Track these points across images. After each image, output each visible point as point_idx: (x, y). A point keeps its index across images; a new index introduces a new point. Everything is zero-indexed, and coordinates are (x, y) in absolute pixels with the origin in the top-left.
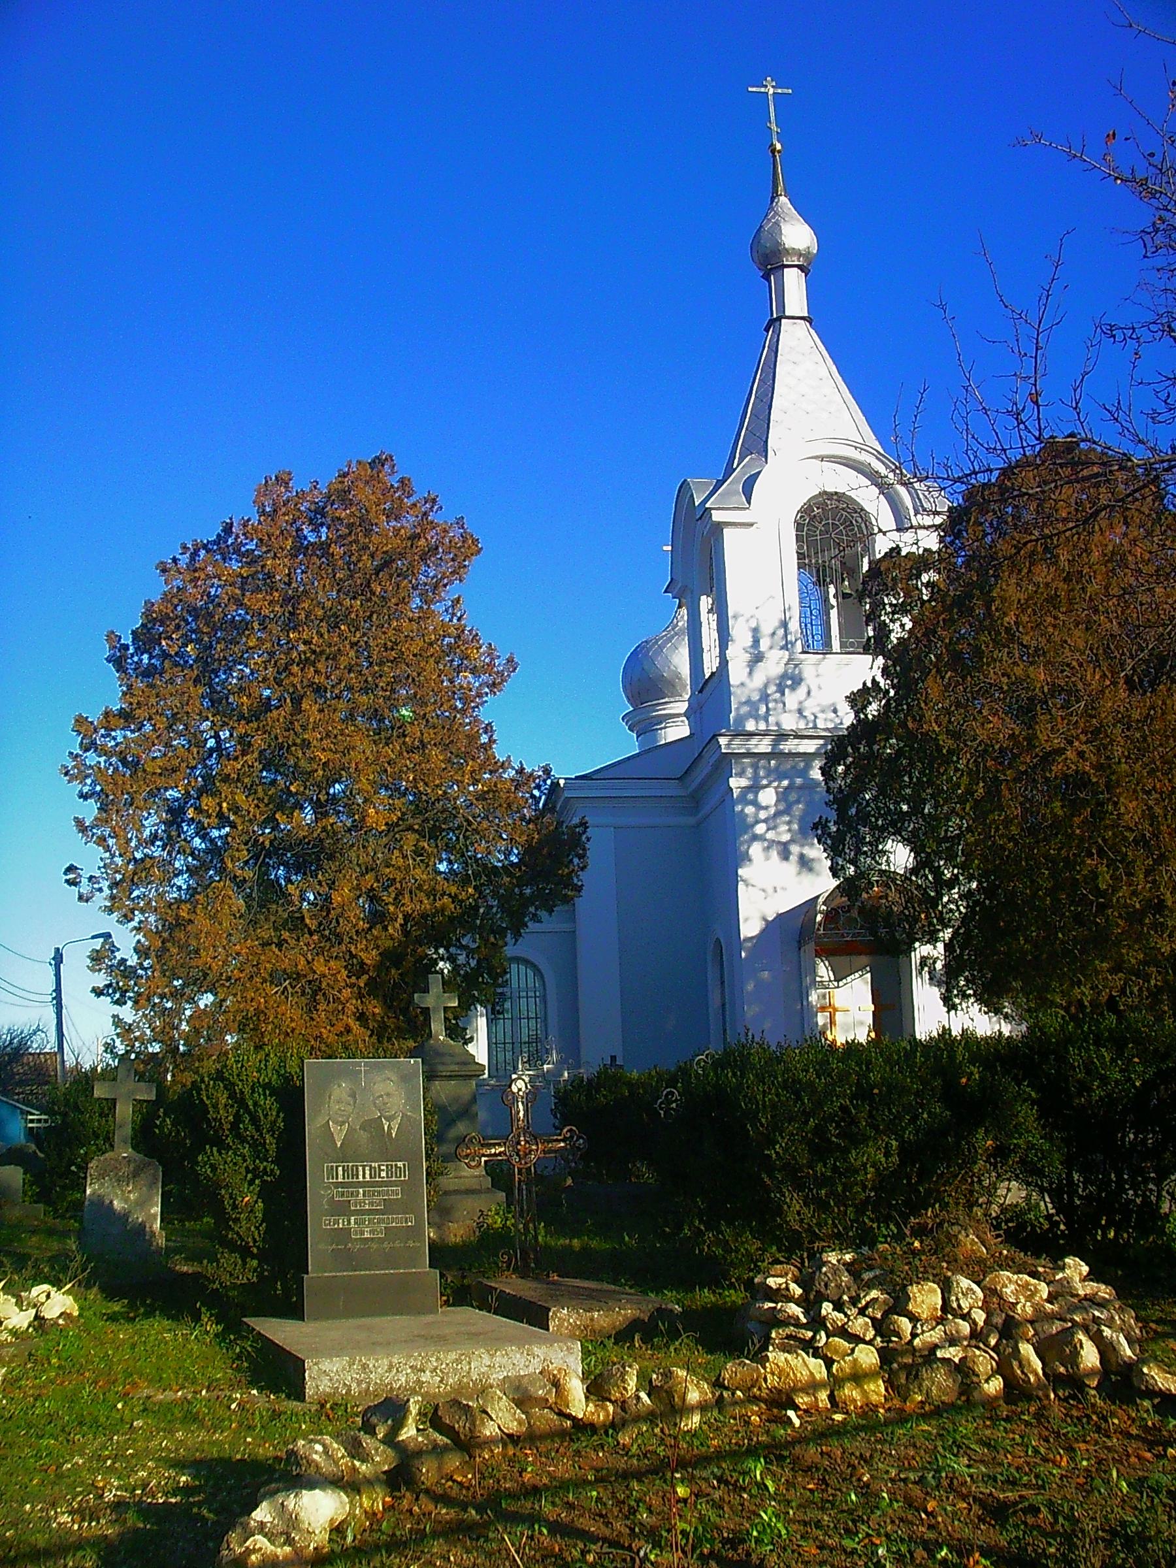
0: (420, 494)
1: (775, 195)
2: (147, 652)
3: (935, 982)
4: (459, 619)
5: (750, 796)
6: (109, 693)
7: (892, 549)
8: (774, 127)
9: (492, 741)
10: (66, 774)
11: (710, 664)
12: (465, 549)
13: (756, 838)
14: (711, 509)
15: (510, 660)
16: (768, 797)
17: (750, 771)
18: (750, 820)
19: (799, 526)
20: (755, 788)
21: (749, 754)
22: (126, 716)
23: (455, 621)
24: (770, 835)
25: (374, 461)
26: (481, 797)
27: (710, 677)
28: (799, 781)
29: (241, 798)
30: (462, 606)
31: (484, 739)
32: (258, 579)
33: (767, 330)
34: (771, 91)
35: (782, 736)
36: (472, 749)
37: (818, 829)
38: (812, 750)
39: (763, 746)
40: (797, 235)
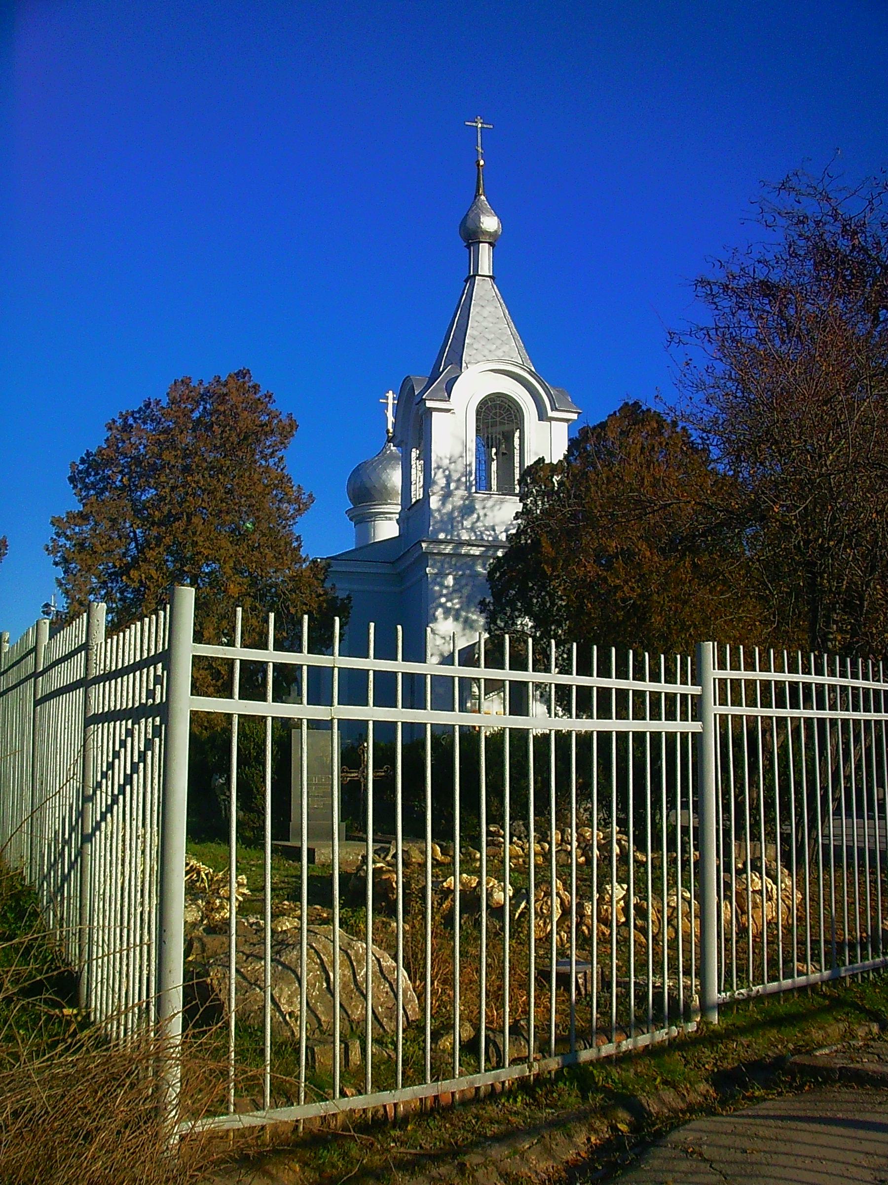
0: (263, 392)
1: (477, 195)
2: (90, 474)
3: (543, 699)
4: (282, 470)
5: (438, 580)
6: (71, 502)
7: (540, 459)
8: (480, 149)
9: (300, 546)
10: (47, 550)
11: (417, 493)
12: (288, 430)
13: (441, 605)
14: (425, 399)
15: (310, 496)
16: (450, 581)
17: (439, 564)
18: (437, 595)
19: (478, 413)
20: (442, 575)
21: (439, 554)
22: (84, 517)
23: (279, 470)
24: (449, 604)
25: (238, 373)
26: (292, 578)
27: (416, 502)
28: (468, 572)
29: (153, 572)
30: (285, 462)
31: (295, 544)
32: (166, 440)
33: (466, 281)
34: (480, 125)
35: (462, 544)
36: (287, 550)
37: (483, 607)
38: (478, 553)
39: (448, 549)
40: (490, 223)
